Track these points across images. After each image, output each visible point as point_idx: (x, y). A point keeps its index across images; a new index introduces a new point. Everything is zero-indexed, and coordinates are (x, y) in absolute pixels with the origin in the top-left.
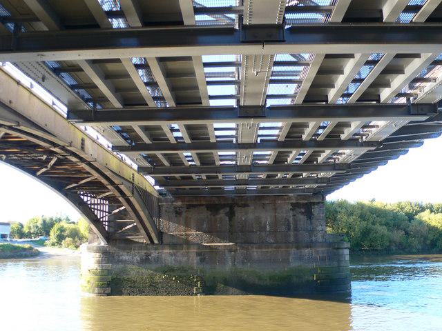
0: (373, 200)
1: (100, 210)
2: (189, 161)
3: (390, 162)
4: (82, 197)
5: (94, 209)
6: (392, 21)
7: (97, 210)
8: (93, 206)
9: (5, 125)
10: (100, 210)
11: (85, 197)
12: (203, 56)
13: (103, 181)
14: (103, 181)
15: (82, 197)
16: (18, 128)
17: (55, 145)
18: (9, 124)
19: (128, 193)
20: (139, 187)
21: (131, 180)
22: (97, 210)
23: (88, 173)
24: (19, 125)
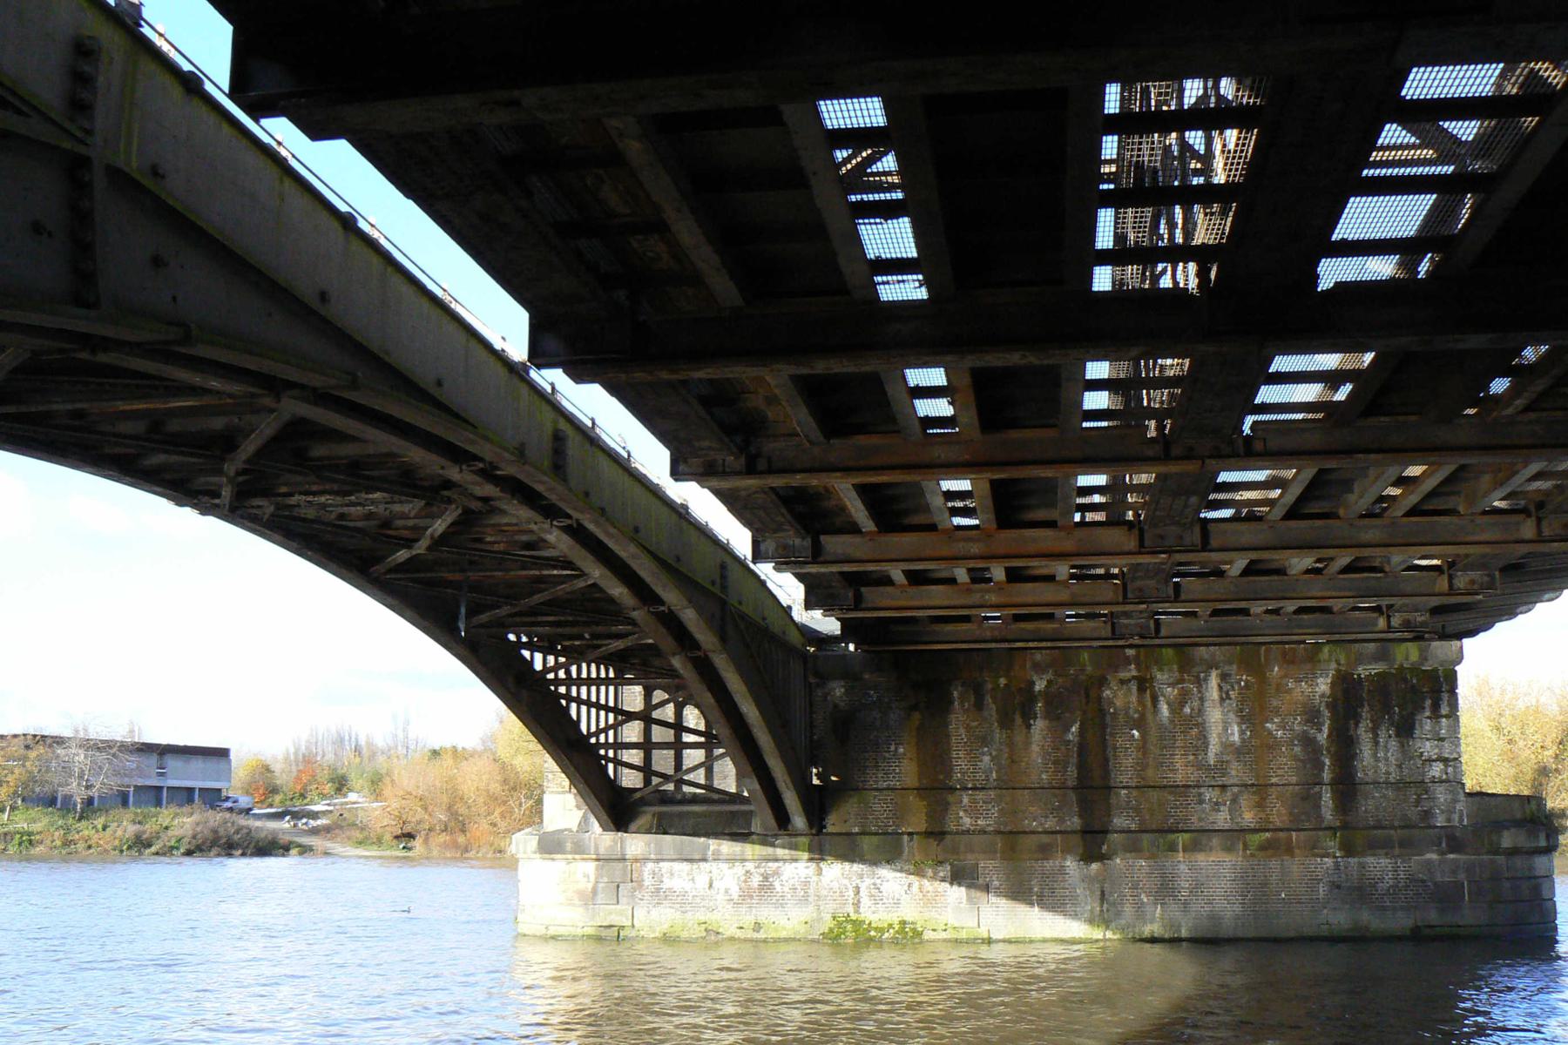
0: (37, 228)
1: (589, 704)
2: (956, 512)
3: (188, 509)
4: (526, 654)
5: (569, 698)
6: (715, 777)
7: (579, 701)
8: (562, 690)
9: (303, 387)
10: (589, 704)
11: (538, 657)
12: (1078, 485)
13: (618, 590)
14: (618, 590)
15: (526, 654)
16: (346, 395)
17: (458, 455)
18: (317, 381)
19: (705, 637)
20: (743, 616)
21: (716, 590)
22: (579, 701)
23: (568, 564)
24: (354, 385)
